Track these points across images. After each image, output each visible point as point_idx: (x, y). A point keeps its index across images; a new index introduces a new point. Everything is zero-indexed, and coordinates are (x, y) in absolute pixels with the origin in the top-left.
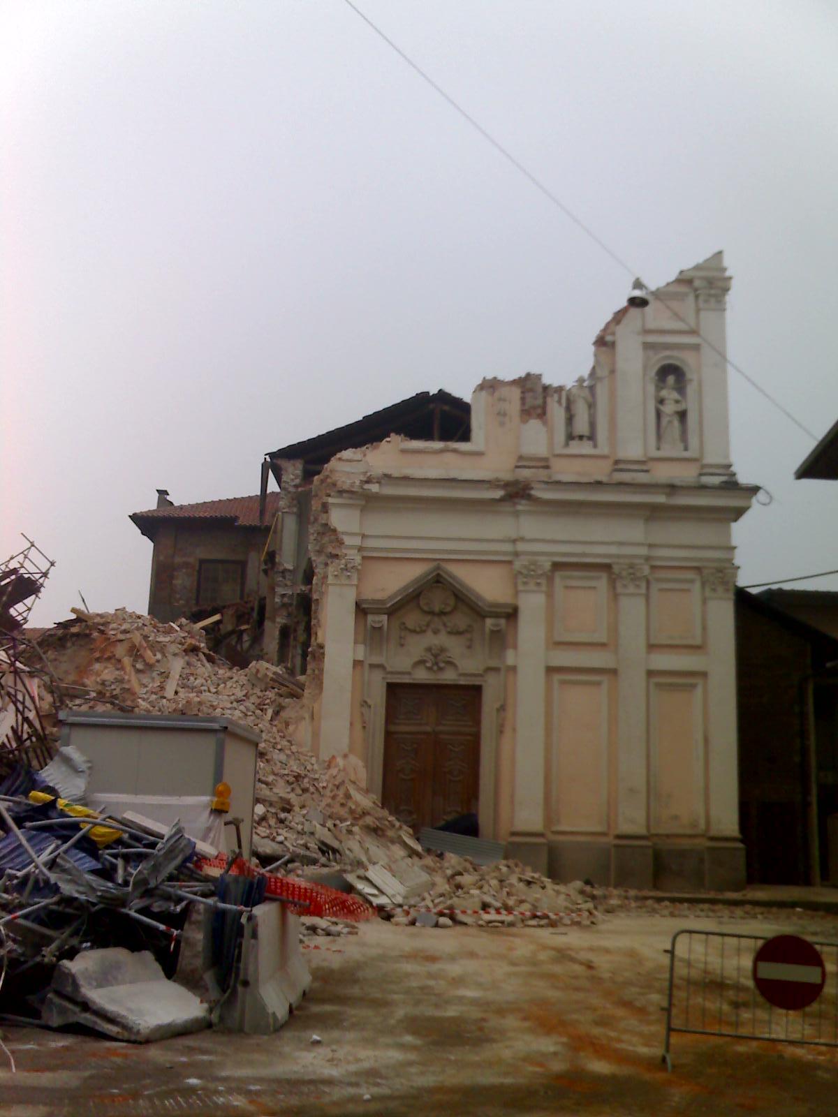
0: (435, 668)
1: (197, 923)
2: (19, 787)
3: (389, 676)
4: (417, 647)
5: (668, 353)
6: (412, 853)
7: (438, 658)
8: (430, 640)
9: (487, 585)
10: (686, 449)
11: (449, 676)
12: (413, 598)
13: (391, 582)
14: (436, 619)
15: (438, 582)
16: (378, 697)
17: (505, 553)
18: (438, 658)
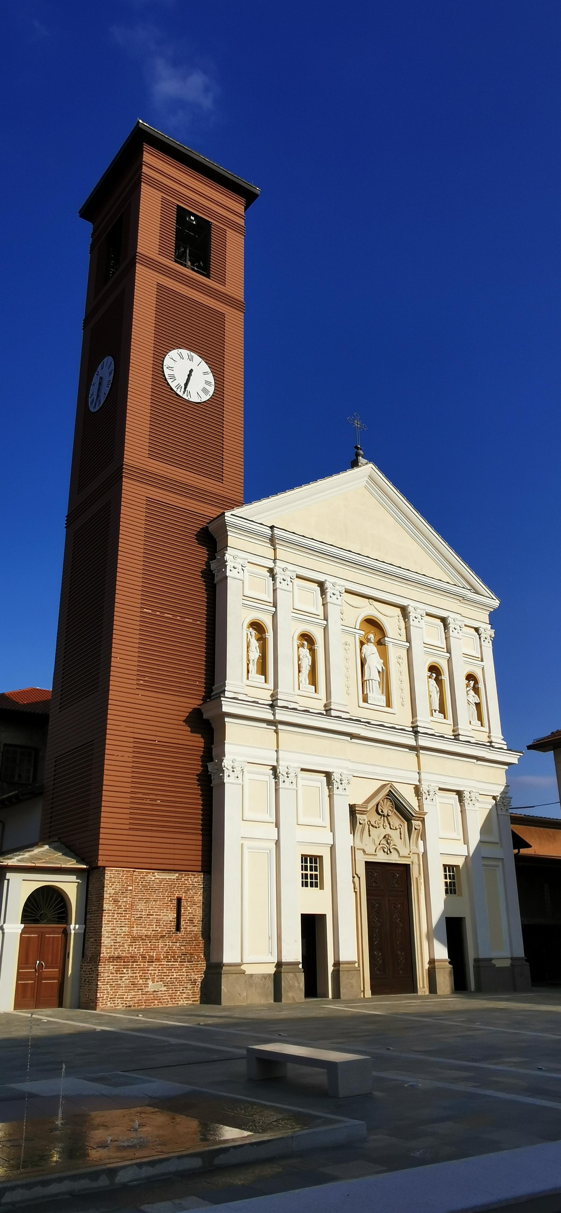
8: (382, 832)
11: (394, 858)
16: (361, 871)
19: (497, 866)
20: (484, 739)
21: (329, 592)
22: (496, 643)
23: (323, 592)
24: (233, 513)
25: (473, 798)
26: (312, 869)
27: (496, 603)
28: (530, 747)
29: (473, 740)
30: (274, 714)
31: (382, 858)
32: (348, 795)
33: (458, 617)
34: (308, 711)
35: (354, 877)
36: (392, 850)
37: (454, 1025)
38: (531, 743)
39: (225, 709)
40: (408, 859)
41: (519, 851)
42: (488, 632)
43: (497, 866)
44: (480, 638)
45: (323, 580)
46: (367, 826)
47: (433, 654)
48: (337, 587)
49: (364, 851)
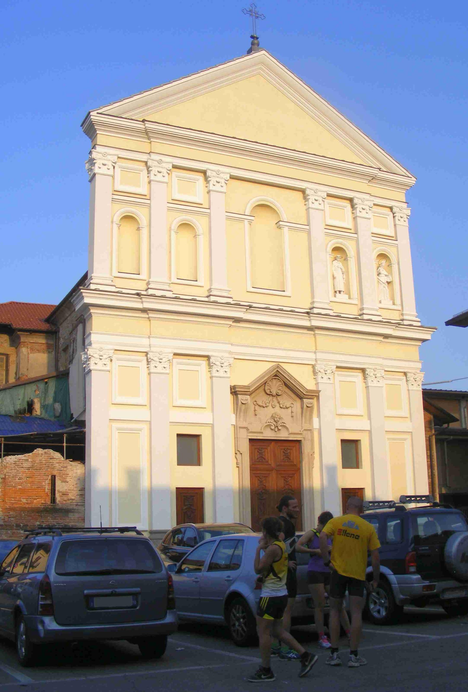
0: (276, 429)
1: (416, 505)
2: (267, 465)
3: (250, 434)
4: (266, 414)
5: (340, 240)
6: (405, 499)
7: (276, 423)
8: (270, 411)
9: (305, 380)
10: (394, 304)
11: (283, 435)
12: (262, 386)
13: (248, 375)
14: (275, 399)
15: (276, 376)
16: (245, 447)
17: (311, 360)
18: (276, 423)
19: (405, 439)
20: (395, 316)
21: (359, 207)
22: (412, 220)
23: (305, 198)
24: (100, 111)
25: (378, 375)
26: (189, 448)
27: (412, 181)
28: (448, 323)
29: (331, 313)
30: (311, 323)
31: (269, 435)
32: (229, 378)
33: (367, 197)
34: (282, 310)
35: (236, 454)
36: (280, 428)
37: (132, 588)
38: (451, 318)
39: (87, 300)
40: (299, 436)
41: (448, 426)
42: (404, 211)
43: (405, 439)
44: (394, 217)
45: (304, 188)
46: (252, 407)
47: (381, 243)
48: (319, 193)
49: (248, 429)
